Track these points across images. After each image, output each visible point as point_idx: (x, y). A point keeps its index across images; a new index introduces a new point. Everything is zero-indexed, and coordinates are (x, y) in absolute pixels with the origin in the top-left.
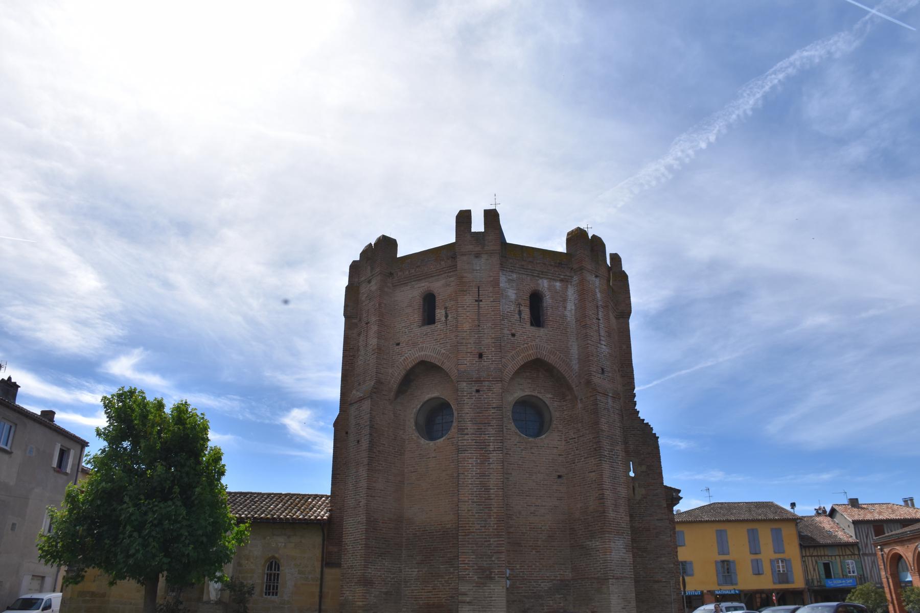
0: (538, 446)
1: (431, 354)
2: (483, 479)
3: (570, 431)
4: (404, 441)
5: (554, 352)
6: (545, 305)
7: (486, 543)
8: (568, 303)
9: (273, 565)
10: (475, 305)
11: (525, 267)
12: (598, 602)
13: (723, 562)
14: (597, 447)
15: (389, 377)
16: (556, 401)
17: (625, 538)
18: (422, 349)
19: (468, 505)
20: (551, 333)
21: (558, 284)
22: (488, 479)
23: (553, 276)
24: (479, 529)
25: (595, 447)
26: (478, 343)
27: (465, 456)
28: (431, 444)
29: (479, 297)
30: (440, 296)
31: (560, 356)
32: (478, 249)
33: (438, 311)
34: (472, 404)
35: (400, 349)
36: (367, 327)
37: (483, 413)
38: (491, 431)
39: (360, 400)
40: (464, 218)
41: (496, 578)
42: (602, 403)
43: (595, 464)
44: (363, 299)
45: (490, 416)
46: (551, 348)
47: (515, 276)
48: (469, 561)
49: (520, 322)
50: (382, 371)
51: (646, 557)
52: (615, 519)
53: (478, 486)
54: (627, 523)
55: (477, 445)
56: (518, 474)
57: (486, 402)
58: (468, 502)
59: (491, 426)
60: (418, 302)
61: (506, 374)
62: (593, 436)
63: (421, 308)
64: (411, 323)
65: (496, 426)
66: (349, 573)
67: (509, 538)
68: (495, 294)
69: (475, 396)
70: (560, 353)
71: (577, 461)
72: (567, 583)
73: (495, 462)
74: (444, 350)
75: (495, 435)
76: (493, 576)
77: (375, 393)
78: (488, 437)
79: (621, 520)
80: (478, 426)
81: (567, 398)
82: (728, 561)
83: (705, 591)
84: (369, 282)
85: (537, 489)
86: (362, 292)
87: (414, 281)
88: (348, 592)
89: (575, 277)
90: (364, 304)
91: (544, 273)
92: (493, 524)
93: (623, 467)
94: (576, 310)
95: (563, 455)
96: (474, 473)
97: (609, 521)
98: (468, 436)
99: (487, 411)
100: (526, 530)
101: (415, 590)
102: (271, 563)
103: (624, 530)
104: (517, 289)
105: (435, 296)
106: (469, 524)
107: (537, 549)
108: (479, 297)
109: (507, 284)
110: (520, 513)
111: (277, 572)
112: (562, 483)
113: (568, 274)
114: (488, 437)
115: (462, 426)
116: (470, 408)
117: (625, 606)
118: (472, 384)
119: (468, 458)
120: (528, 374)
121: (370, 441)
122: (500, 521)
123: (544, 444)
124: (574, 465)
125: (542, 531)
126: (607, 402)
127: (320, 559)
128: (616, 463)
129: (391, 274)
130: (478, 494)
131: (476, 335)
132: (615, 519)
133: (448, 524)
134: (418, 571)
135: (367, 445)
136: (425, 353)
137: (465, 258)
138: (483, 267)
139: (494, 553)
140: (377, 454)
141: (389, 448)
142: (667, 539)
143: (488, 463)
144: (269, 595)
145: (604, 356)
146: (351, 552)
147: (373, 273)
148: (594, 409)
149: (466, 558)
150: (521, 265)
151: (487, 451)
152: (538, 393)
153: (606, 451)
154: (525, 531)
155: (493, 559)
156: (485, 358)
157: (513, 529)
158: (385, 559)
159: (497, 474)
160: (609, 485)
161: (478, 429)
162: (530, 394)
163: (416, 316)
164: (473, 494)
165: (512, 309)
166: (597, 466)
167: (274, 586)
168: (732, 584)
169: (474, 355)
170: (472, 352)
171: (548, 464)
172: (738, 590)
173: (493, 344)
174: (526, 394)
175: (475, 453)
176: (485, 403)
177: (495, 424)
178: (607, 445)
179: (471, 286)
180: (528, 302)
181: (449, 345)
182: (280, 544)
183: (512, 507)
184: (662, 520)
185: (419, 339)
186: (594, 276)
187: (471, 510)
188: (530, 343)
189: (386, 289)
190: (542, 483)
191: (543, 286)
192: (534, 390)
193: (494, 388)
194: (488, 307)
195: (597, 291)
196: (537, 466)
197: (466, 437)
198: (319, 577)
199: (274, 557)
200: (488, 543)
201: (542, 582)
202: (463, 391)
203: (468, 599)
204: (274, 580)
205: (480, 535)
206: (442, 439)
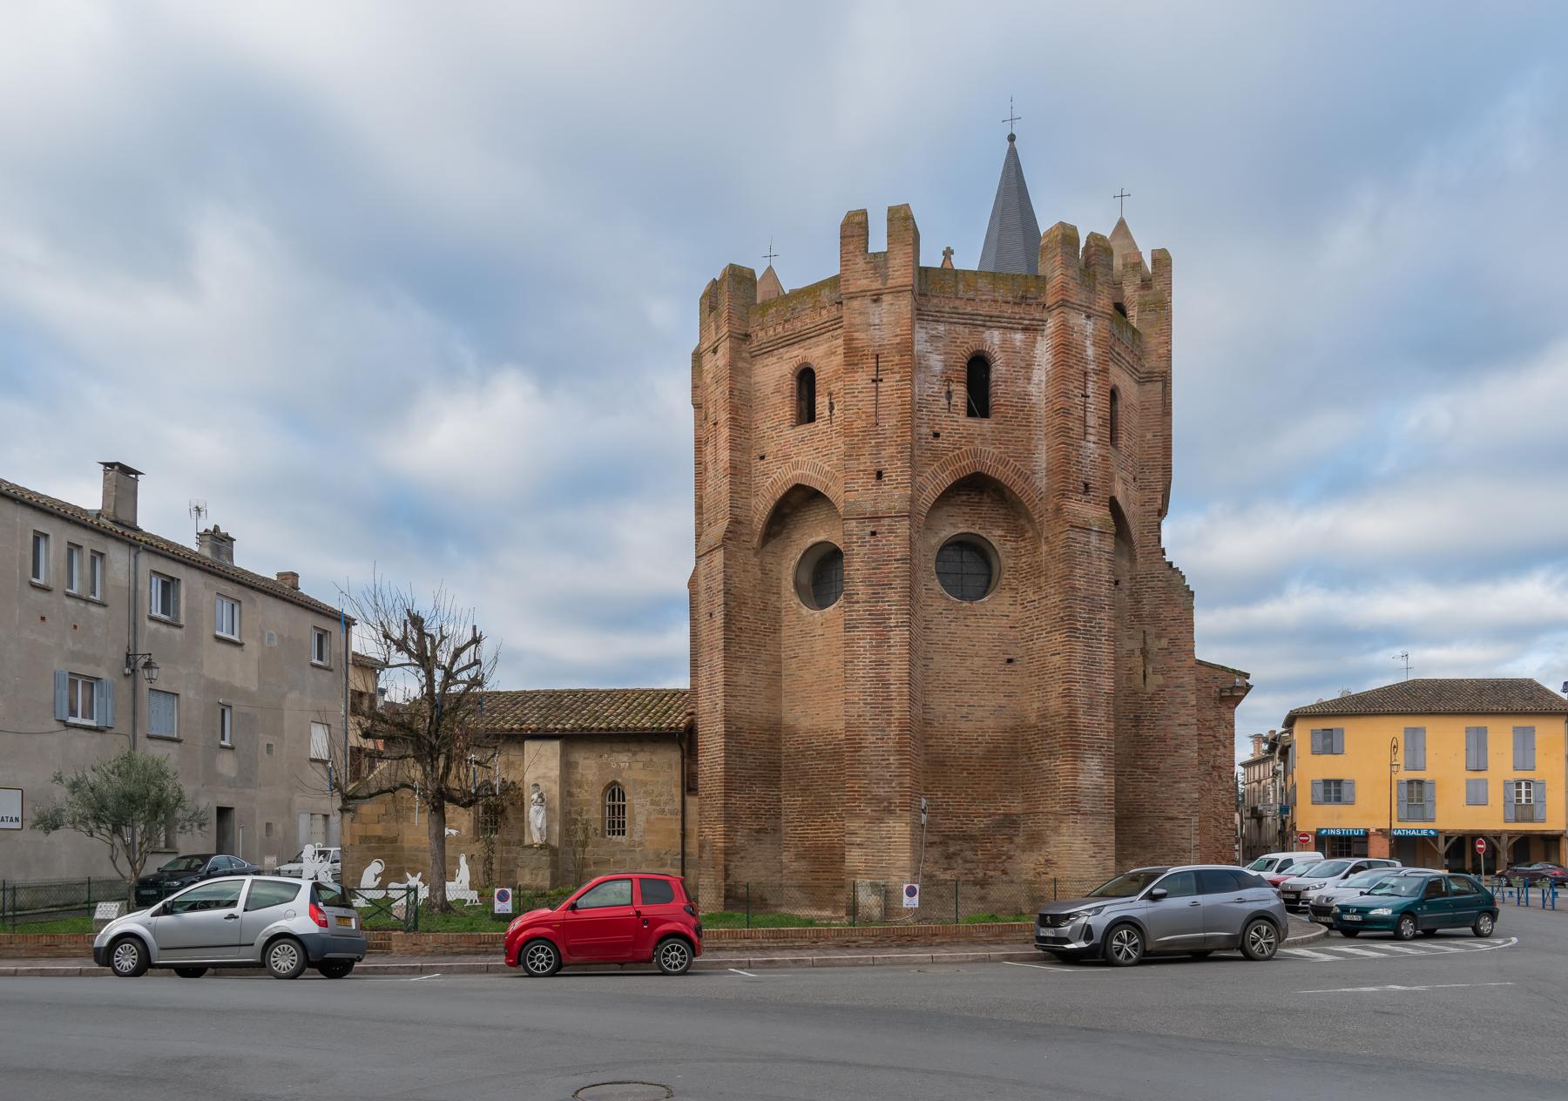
0: (976, 615)
1: (811, 473)
2: (881, 669)
3: (1028, 589)
4: (780, 612)
5: (1005, 459)
6: (993, 376)
7: (884, 763)
8: (1034, 371)
9: (614, 792)
10: (871, 388)
11: (961, 311)
12: (1056, 847)
13: (1410, 782)
14: (1065, 616)
15: (752, 512)
16: (1010, 541)
17: (1104, 755)
18: (797, 465)
19: (859, 708)
20: (1001, 426)
21: (1019, 337)
22: (888, 669)
23: (1010, 323)
24: (874, 743)
25: (1061, 615)
26: (875, 454)
27: (855, 635)
28: (816, 616)
29: (877, 375)
30: (821, 373)
31: (1016, 466)
32: (876, 285)
33: (818, 399)
34: (865, 554)
35: (765, 466)
36: (715, 430)
37: (881, 569)
38: (894, 596)
39: (711, 551)
40: (855, 228)
41: (898, 812)
42: (1077, 543)
43: (1060, 642)
44: (708, 380)
45: (890, 573)
46: (1000, 452)
47: (943, 329)
48: (859, 787)
49: (949, 412)
50: (740, 503)
51: (1156, 782)
52: (1088, 727)
53: (873, 681)
54: (1108, 733)
55: (871, 619)
56: (943, 659)
57: (886, 550)
58: (859, 703)
59: (893, 588)
60: (789, 385)
61: (923, 503)
62: (1061, 598)
63: (795, 394)
64: (780, 421)
65: (901, 588)
66: (707, 804)
67: (926, 754)
68: (904, 368)
69: (870, 542)
70: (1015, 461)
71: (1035, 637)
72: (1015, 818)
73: (898, 644)
74: (829, 466)
75: (898, 603)
76: (893, 808)
77: (730, 539)
78: (889, 606)
79: (1099, 728)
80: (874, 589)
81: (1027, 535)
82: (1420, 782)
83: (1373, 830)
84: (715, 351)
85: (973, 681)
86: (706, 368)
87: (783, 347)
88: (707, 830)
89: (1049, 321)
90: (709, 391)
91: (993, 319)
92: (894, 735)
93: (1109, 645)
94: (1047, 382)
95: (1016, 628)
96: (868, 660)
97: (1077, 730)
98: (858, 605)
99: (887, 565)
100: (953, 743)
101: (800, 826)
102: (614, 791)
103: (1102, 743)
104: (945, 353)
105: (814, 374)
106: (859, 735)
107: (969, 770)
108: (877, 375)
109: (928, 344)
110: (944, 717)
111: (621, 803)
112: (1013, 671)
113: (1037, 316)
114: (889, 606)
115: (850, 590)
116: (862, 562)
117: (1095, 853)
118: (864, 522)
119: (858, 639)
120: (964, 498)
121: (724, 614)
122: (904, 730)
123: (987, 611)
124: (1031, 643)
125: (979, 743)
126: (1088, 541)
127: (680, 783)
128: (1097, 639)
129: (748, 336)
130: (873, 692)
131: (873, 441)
132: (1088, 727)
133: (841, 734)
134: (802, 801)
135: (723, 621)
136: (801, 472)
137: (856, 304)
138: (885, 320)
139: (895, 776)
140: (738, 633)
141: (756, 623)
142: (1192, 755)
143: (888, 646)
144: (614, 834)
145: (1091, 461)
146: (710, 775)
147: (719, 336)
148: (1064, 554)
149: (855, 783)
150: (953, 308)
151: (886, 627)
152: (980, 528)
153: (1080, 621)
154: (951, 744)
155: (894, 785)
156: (887, 479)
157: (934, 740)
158: (755, 784)
159: (901, 661)
160: (1080, 675)
161: (873, 593)
162: (966, 530)
163: (786, 409)
164: (866, 692)
165: (936, 390)
166: (1063, 646)
167: (619, 822)
168: (1424, 820)
169: (869, 474)
170: (866, 470)
171: (992, 642)
172: (1433, 830)
173: (899, 455)
174: (960, 531)
175: (868, 631)
176: (884, 553)
177: (899, 586)
178: (1082, 611)
179: (864, 355)
180: (964, 375)
181: (835, 459)
182: (622, 765)
183: (933, 709)
184: (1186, 725)
185: (792, 449)
186: (1083, 316)
187: (863, 715)
188: (964, 448)
189: (740, 364)
190: (981, 671)
191: (992, 343)
192: (973, 524)
193: (897, 529)
194: (892, 390)
195: (1088, 343)
196: (974, 646)
197: (856, 606)
198: (680, 808)
199: (615, 783)
200: (887, 762)
201: (976, 817)
202: (850, 535)
203: (858, 840)
204: (619, 814)
205: (875, 751)
206: (831, 608)
